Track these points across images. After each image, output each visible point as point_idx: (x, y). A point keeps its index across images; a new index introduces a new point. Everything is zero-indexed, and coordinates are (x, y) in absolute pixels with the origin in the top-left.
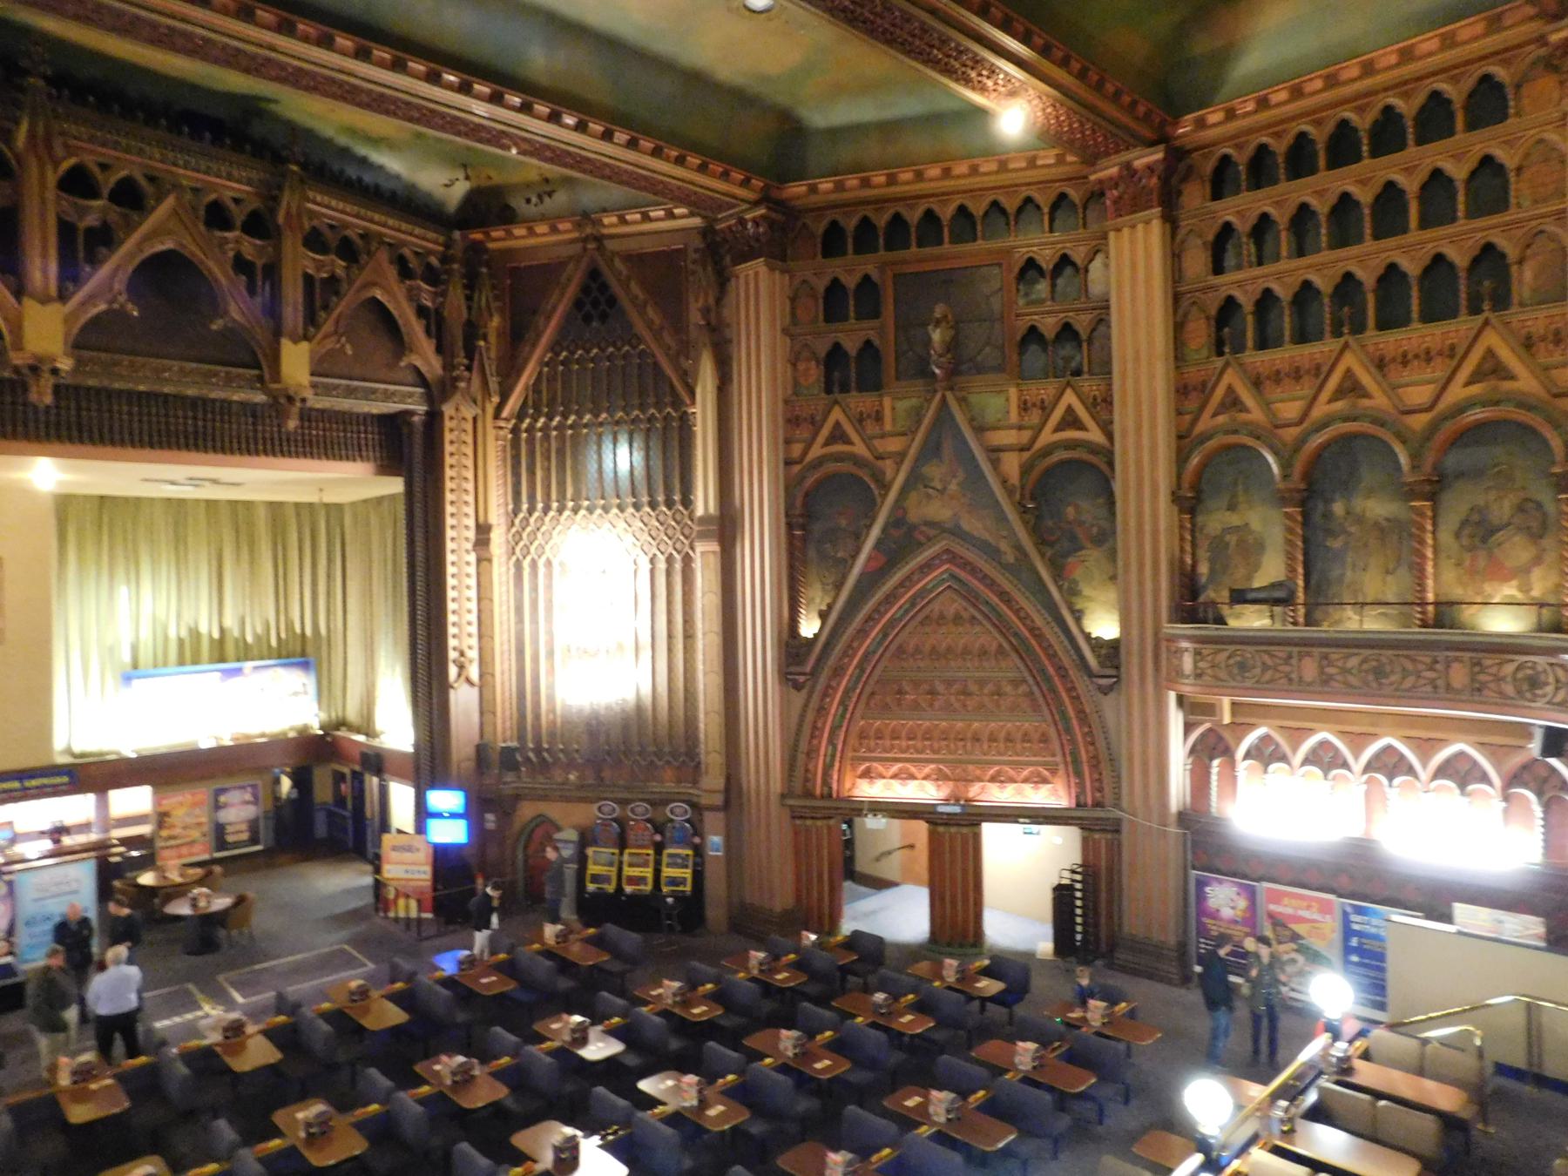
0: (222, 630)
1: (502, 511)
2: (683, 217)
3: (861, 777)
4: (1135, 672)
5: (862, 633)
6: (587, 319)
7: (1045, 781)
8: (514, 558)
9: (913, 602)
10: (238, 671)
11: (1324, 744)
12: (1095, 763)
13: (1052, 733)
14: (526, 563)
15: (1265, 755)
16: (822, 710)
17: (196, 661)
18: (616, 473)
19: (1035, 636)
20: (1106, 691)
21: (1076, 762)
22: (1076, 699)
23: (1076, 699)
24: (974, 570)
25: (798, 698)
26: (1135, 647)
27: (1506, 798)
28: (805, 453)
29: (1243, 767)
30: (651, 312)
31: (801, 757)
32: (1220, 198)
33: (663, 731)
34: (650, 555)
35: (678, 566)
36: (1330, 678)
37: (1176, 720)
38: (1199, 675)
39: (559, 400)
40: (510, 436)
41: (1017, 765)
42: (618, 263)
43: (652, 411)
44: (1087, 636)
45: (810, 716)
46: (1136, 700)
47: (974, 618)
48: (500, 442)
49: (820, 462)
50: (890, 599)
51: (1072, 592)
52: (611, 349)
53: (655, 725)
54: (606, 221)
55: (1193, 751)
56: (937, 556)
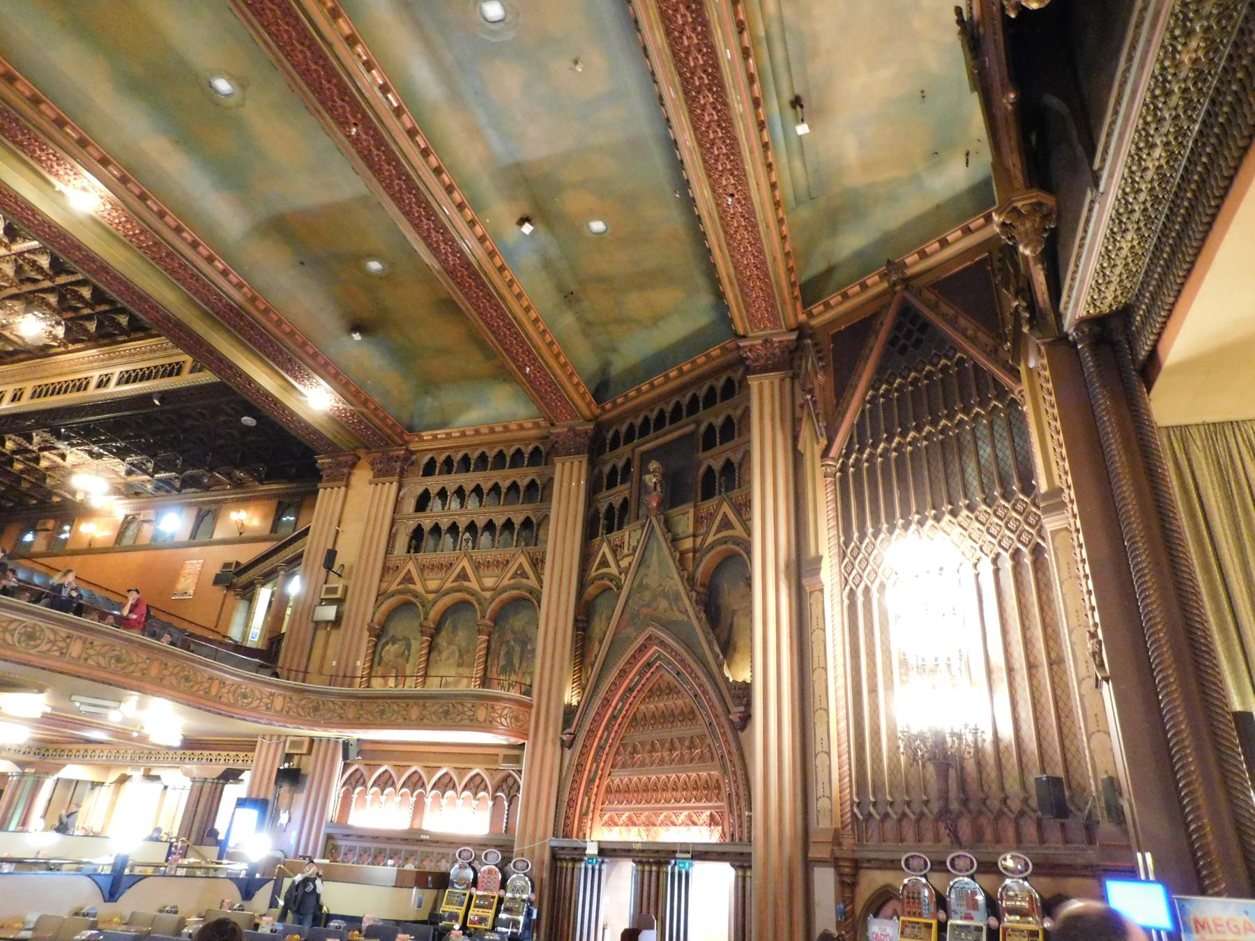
1: (834, 542)
2: (957, 240)
6: (903, 350)
8: (848, 588)
14: (859, 592)
16: (580, 767)
28: (703, 541)
30: (962, 322)
34: (992, 555)
35: (1027, 560)
39: (883, 427)
40: (838, 474)
42: (928, 295)
43: (960, 416)
48: (829, 479)
49: (712, 547)
52: (913, 374)
54: (908, 261)
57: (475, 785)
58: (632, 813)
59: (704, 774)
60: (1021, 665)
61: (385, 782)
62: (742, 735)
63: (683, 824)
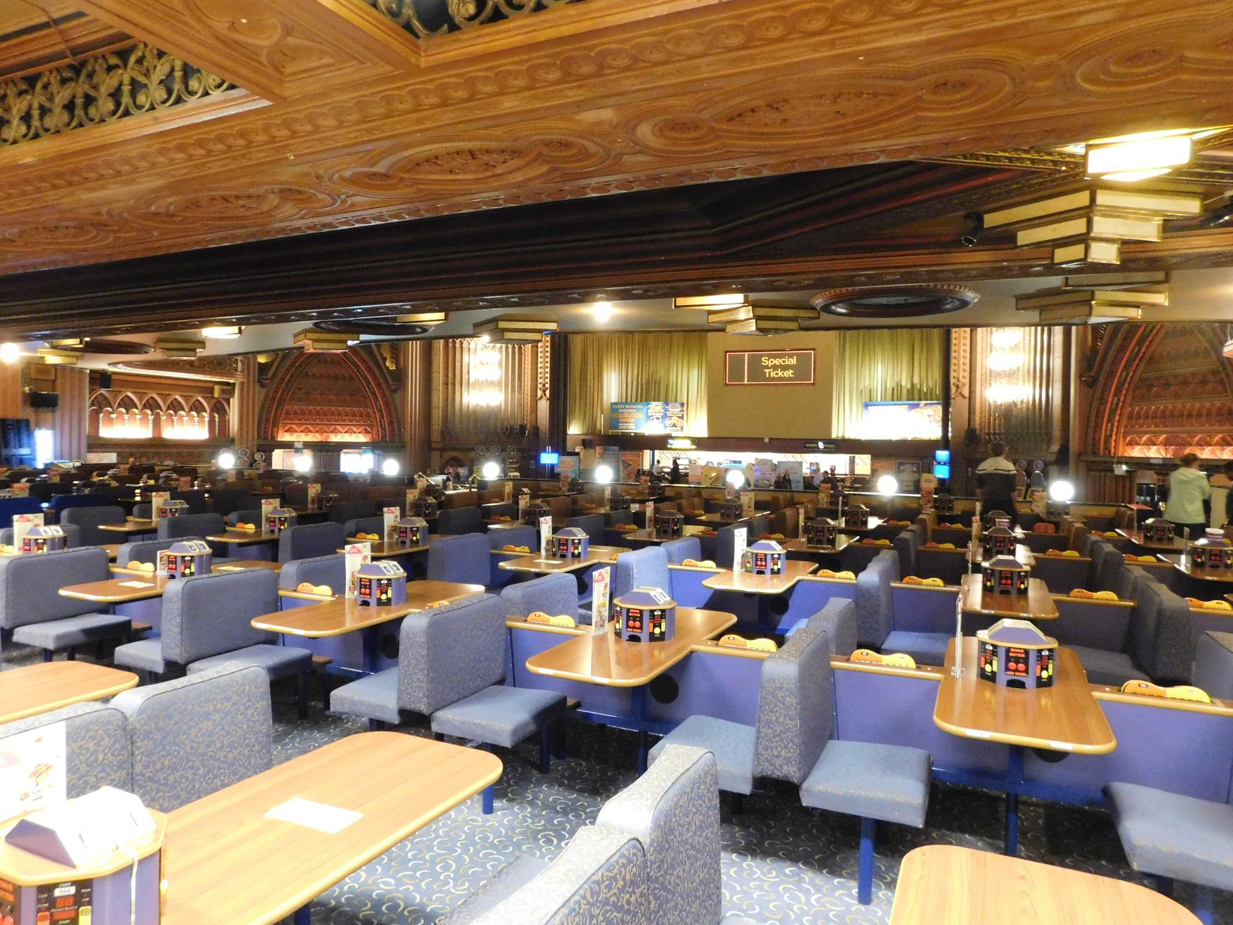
0: (913, 385)
10: (917, 406)
16: (1102, 400)
17: (900, 399)
18: (62, 432)
25: (264, 391)
31: (1091, 431)
32: (725, 819)
33: (492, 425)
45: (1095, 404)
53: (461, 423)
57: (198, 408)
58: (1205, 435)
59: (1218, 404)
60: (682, 182)
61: (128, 405)
62: (397, 396)
63: (1217, 444)
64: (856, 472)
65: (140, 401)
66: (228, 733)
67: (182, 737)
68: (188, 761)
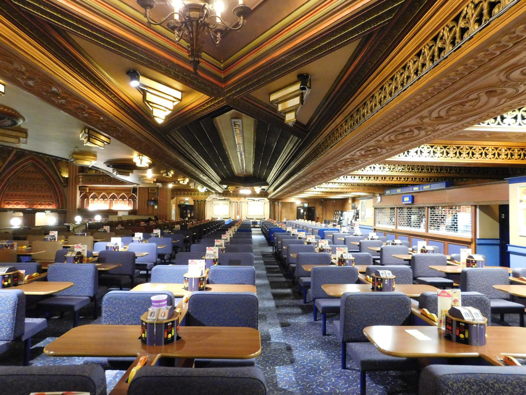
3: (6, 204)
4: (71, 183)
5: (9, 173)
7: (51, 205)
9: (22, 167)
11: (104, 195)
12: (62, 200)
13: (53, 196)
15: (94, 197)
19: (50, 176)
20: (65, 187)
21: (58, 200)
22: (58, 188)
23: (58, 188)
24: (37, 162)
26: (71, 179)
27: (129, 201)
29: (90, 200)
36: (103, 181)
37: (78, 192)
38: (82, 181)
41: (45, 202)
44: (62, 176)
46: (71, 189)
47: (37, 172)
50: (17, 166)
51: (59, 168)
55: (81, 198)
56: (30, 158)
57: (123, 198)
64: (499, 238)
65: (118, 196)
66: (377, 309)
67: (118, 316)
68: (362, 313)
